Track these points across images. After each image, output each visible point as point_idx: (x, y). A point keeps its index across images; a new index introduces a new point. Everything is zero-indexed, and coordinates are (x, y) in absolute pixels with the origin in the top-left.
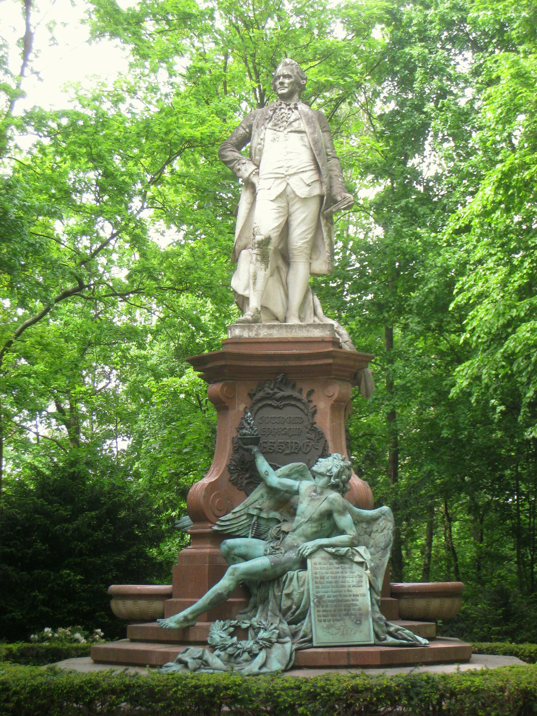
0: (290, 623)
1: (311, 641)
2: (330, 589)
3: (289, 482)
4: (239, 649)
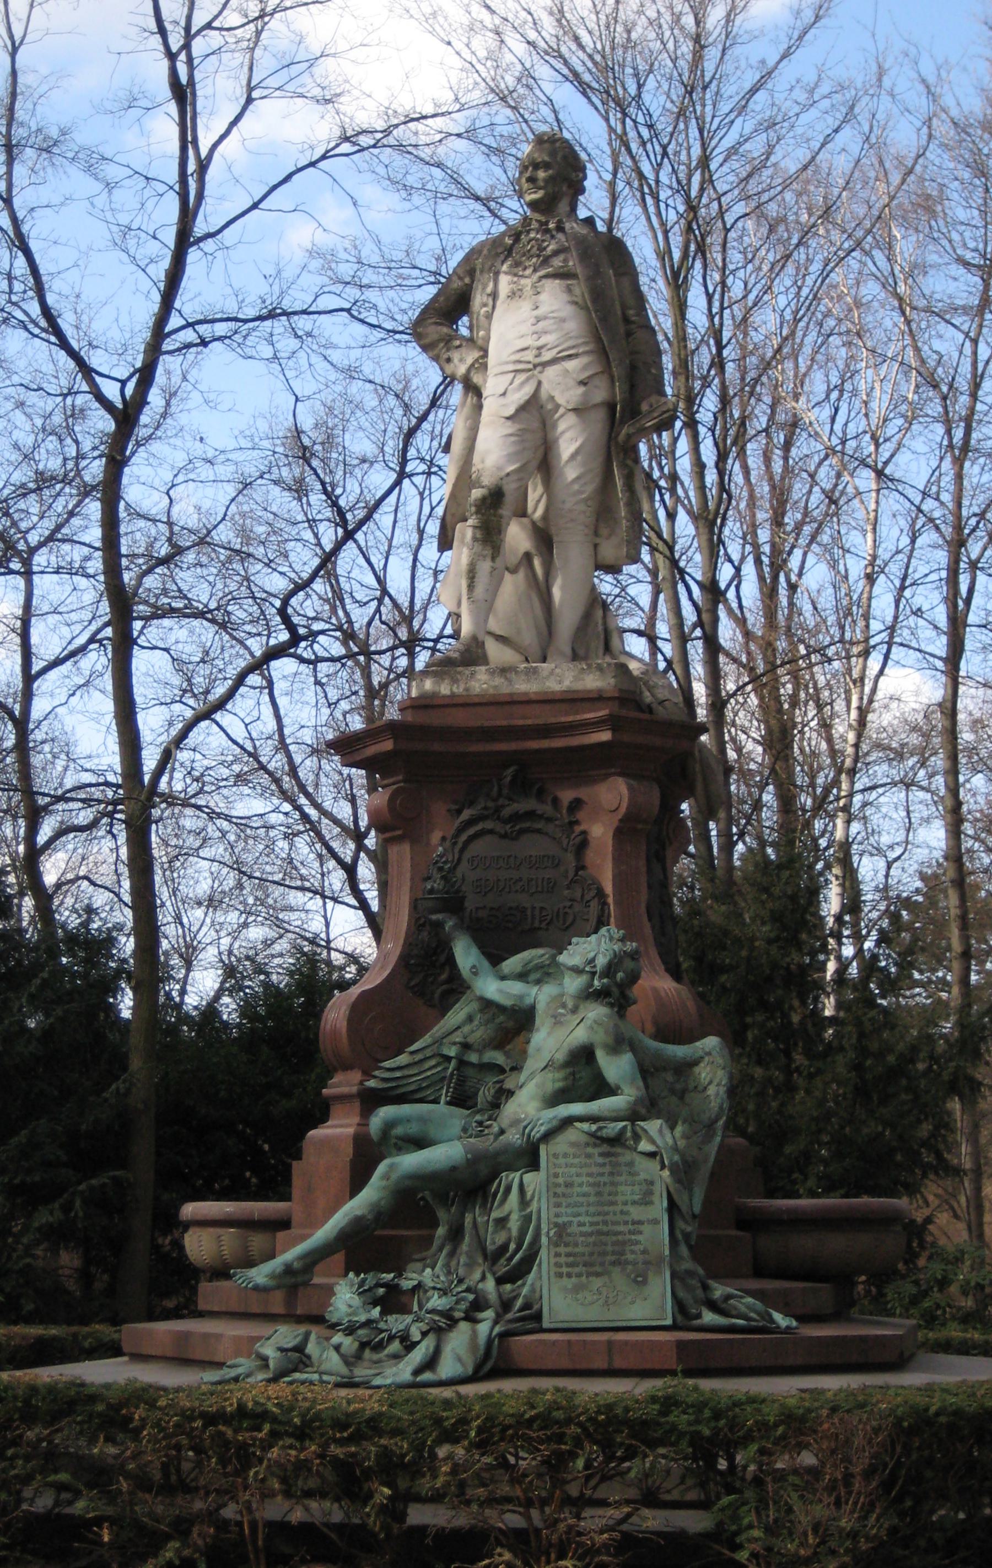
0: (500, 1281)
1: (538, 1317)
2: (582, 1210)
3: (516, 987)
4: (382, 1331)
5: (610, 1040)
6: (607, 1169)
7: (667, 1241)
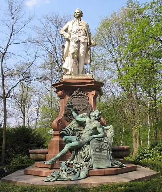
0: (85, 162)
1: (92, 167)
3: (82, 119)
5: (99, 126)
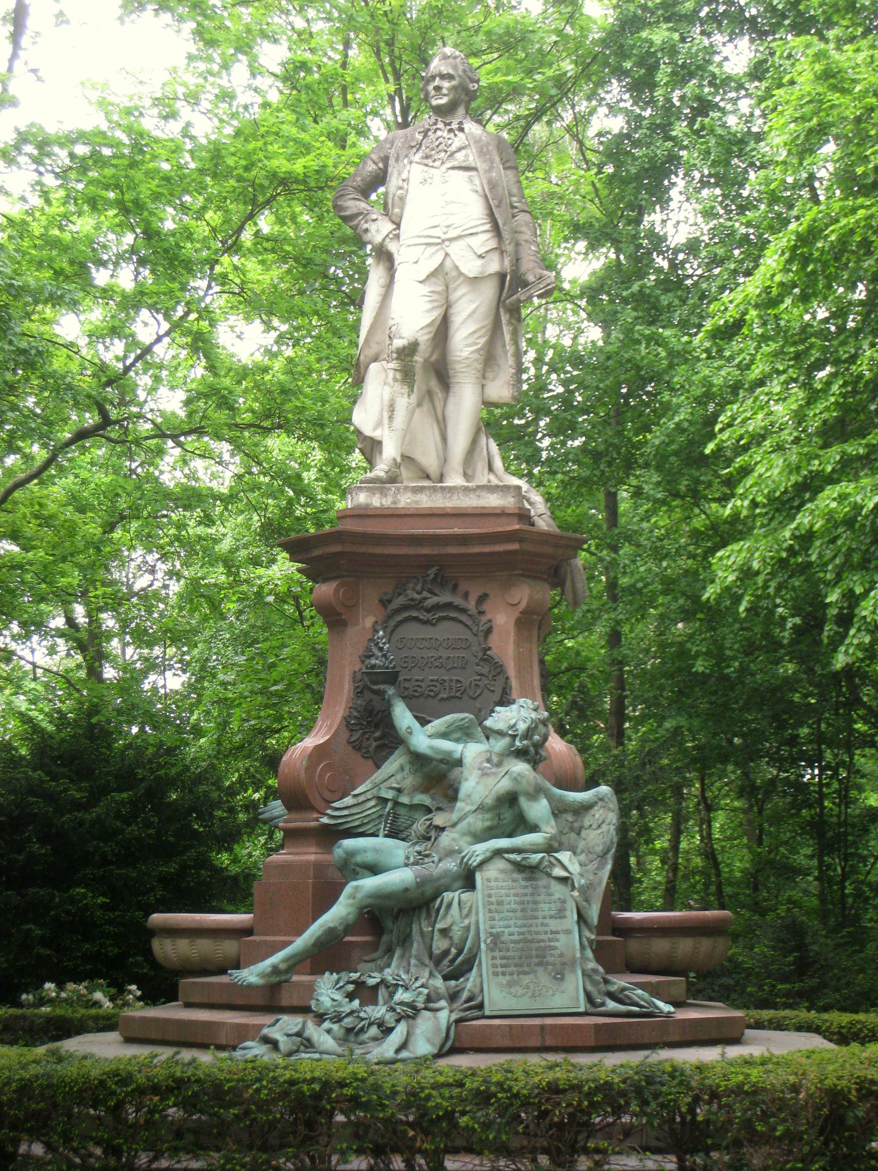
0: (446, 978)
1: (481, 1006)
2: (512, 922)
3: (446, 745)
4: (363, 1019)
6: (529, 891)
7: (578, 947)
